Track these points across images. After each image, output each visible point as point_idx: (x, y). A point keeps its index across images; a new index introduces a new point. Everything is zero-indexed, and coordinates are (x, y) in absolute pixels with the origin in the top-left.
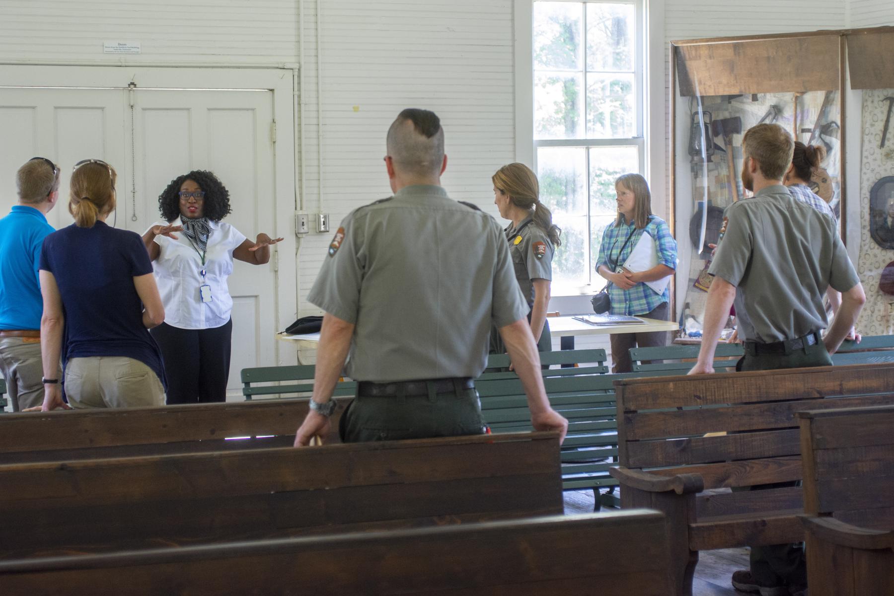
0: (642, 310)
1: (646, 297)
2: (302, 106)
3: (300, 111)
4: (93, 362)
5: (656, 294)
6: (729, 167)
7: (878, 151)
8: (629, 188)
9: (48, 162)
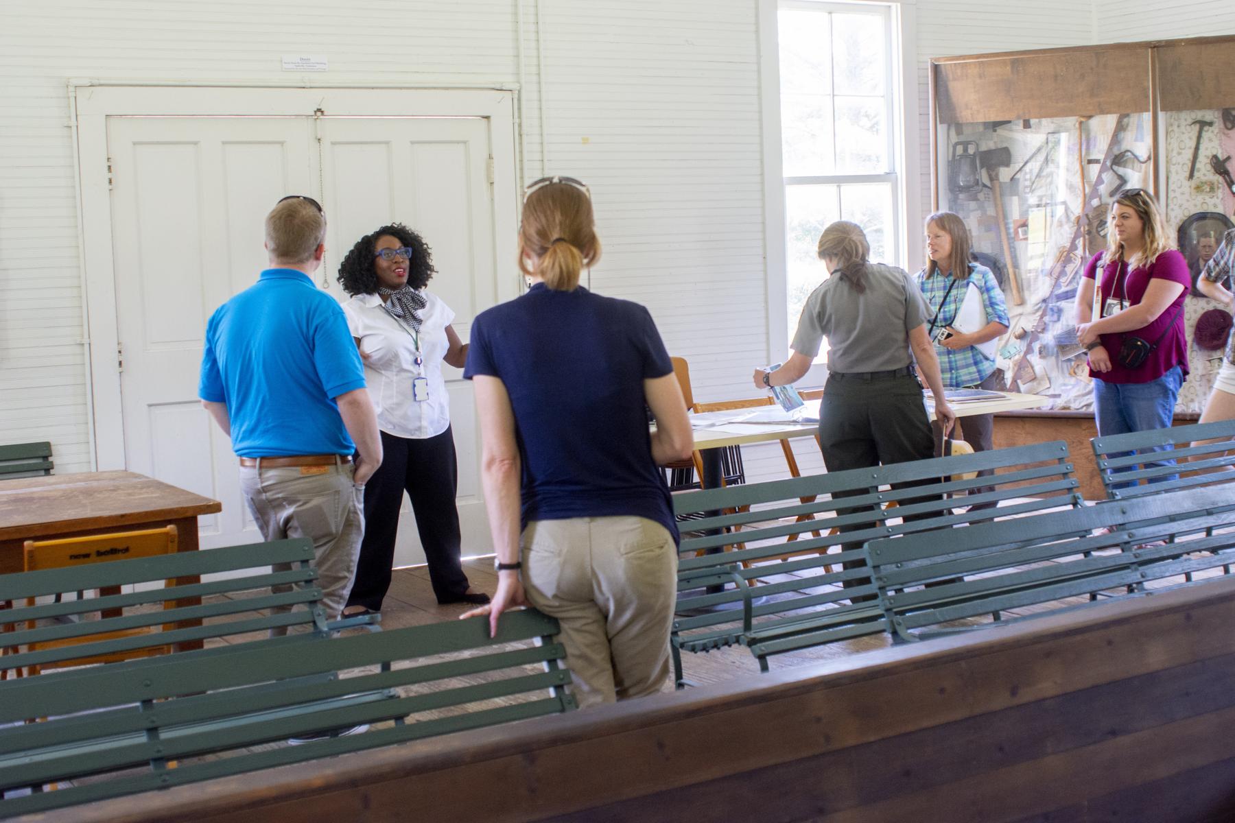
0: (973, 380)
1: (976, 363)
2: (524, 137)
3: (521, 144)
4: (578, 527)
5: (987, 359)
6: (996, 206)
7: (1186, 183)
8: (943, 228)
9: (313, 202)
